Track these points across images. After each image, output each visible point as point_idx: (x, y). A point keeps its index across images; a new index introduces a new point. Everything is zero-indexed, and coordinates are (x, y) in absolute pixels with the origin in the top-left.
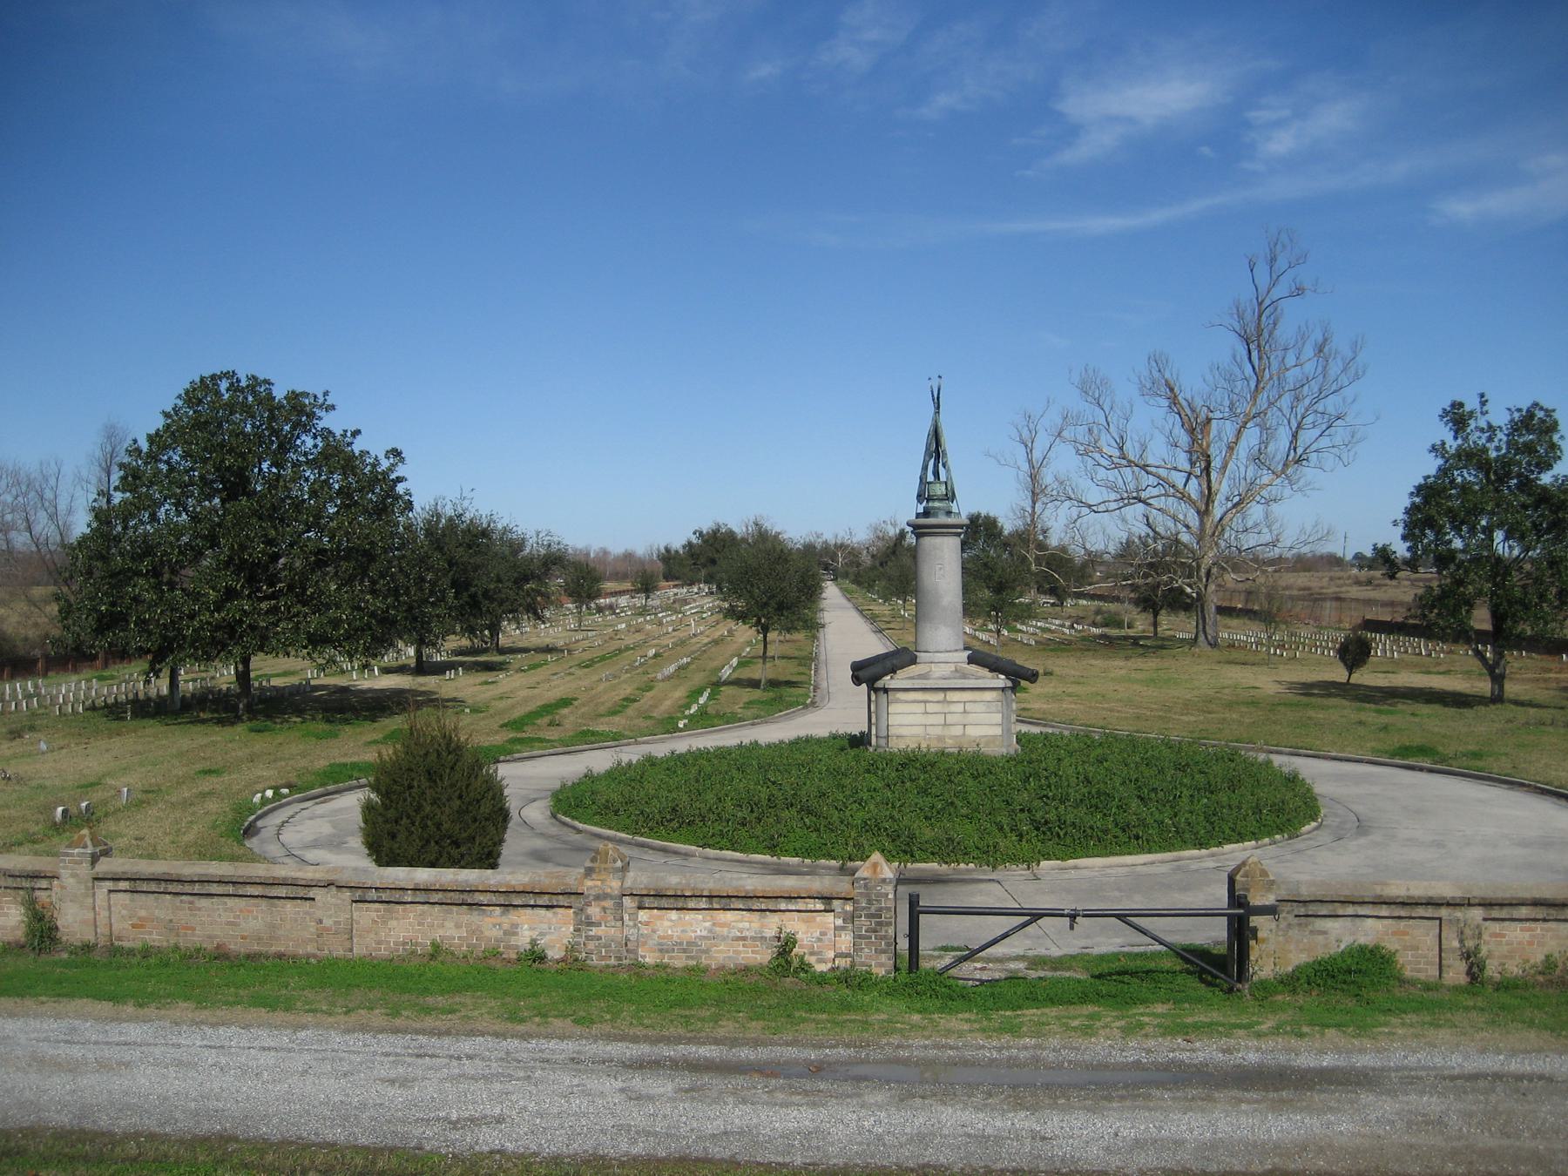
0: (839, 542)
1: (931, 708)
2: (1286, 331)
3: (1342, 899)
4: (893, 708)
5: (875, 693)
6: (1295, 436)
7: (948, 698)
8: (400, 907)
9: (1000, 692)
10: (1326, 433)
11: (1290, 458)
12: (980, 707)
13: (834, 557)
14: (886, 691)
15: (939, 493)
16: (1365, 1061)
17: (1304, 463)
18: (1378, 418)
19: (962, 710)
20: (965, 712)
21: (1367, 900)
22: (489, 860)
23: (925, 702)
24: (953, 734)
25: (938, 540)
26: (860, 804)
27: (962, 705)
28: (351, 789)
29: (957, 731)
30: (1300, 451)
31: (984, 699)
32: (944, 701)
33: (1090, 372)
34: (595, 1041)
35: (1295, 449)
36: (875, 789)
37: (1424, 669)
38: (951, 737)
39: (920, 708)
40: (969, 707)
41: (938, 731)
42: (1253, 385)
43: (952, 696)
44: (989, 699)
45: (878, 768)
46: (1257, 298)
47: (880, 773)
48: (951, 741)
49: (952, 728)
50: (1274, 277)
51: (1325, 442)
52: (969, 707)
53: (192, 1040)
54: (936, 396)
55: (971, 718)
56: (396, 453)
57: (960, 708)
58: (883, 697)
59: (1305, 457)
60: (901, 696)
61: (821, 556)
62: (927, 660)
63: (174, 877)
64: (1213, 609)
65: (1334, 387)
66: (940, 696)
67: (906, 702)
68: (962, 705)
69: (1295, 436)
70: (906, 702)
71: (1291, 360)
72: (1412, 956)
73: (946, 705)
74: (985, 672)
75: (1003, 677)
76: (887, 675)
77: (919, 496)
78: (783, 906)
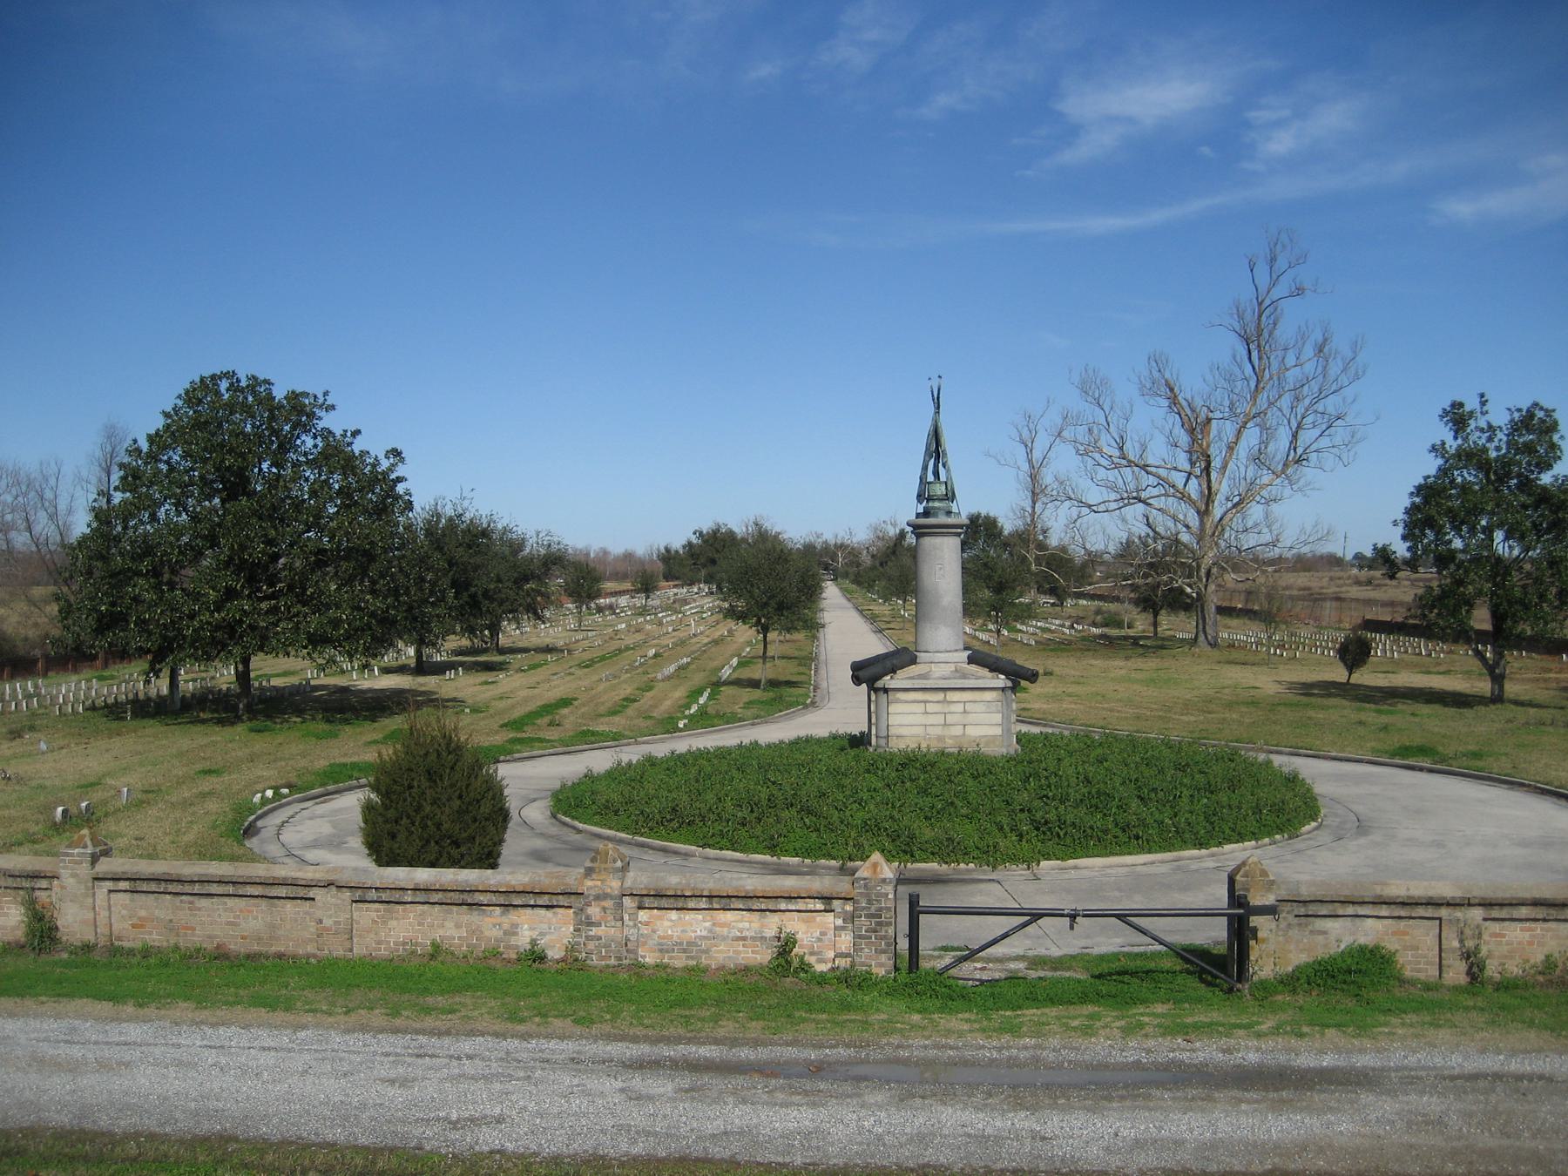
0: (839, 542)
1: (931, 708)
2: (1286, 331)
4: (893, 708)
5: (875, 693)
7: (948, 698)
9: (1000, 692)
10: (1326, 433)
11: (1290, 458)
12: (980, 707)
13: (834, 557)
14: (886, 691)
15: (939, 493)
17: (1304, 463)
18: (1378, 418)
19: (962, 710)
20: (965, 712)
23: (925, 702)
24: (953, 734)
25: (938, 540)
26: (860, 804)
27: (962, 705)
30: (1300, 451)
31: (984, 699)
32: (944, 701)
33: (1090, 372)
35: (1295, 449)
36: (875, 789)
38: (951, 737)
39: (920, 708)
40: (969, 707)
42: (1253, 385)
44: (989, 699)
45: (878, 768)
46: (1257, 298)
48: (951, 741)
49: (952, 728)
50: (1274, 277)
51: (1325, 442)
52: (969, 707)
54: (936, 396)
57: (960, 708)
58: (883, 697)
60: (901, 696)
61: (821, 556)
62: (927, 660)
64: (1213, 609)
65: (1334, 387)
66: (940, 696)
67: (906, 702)
68: (962, 705)
69: (1295, 436)
70: (906, 702)
73: (946, 705)
74: (985, 672)
75: (1003, 677)
76: (887, 675)
77: (919, 496)
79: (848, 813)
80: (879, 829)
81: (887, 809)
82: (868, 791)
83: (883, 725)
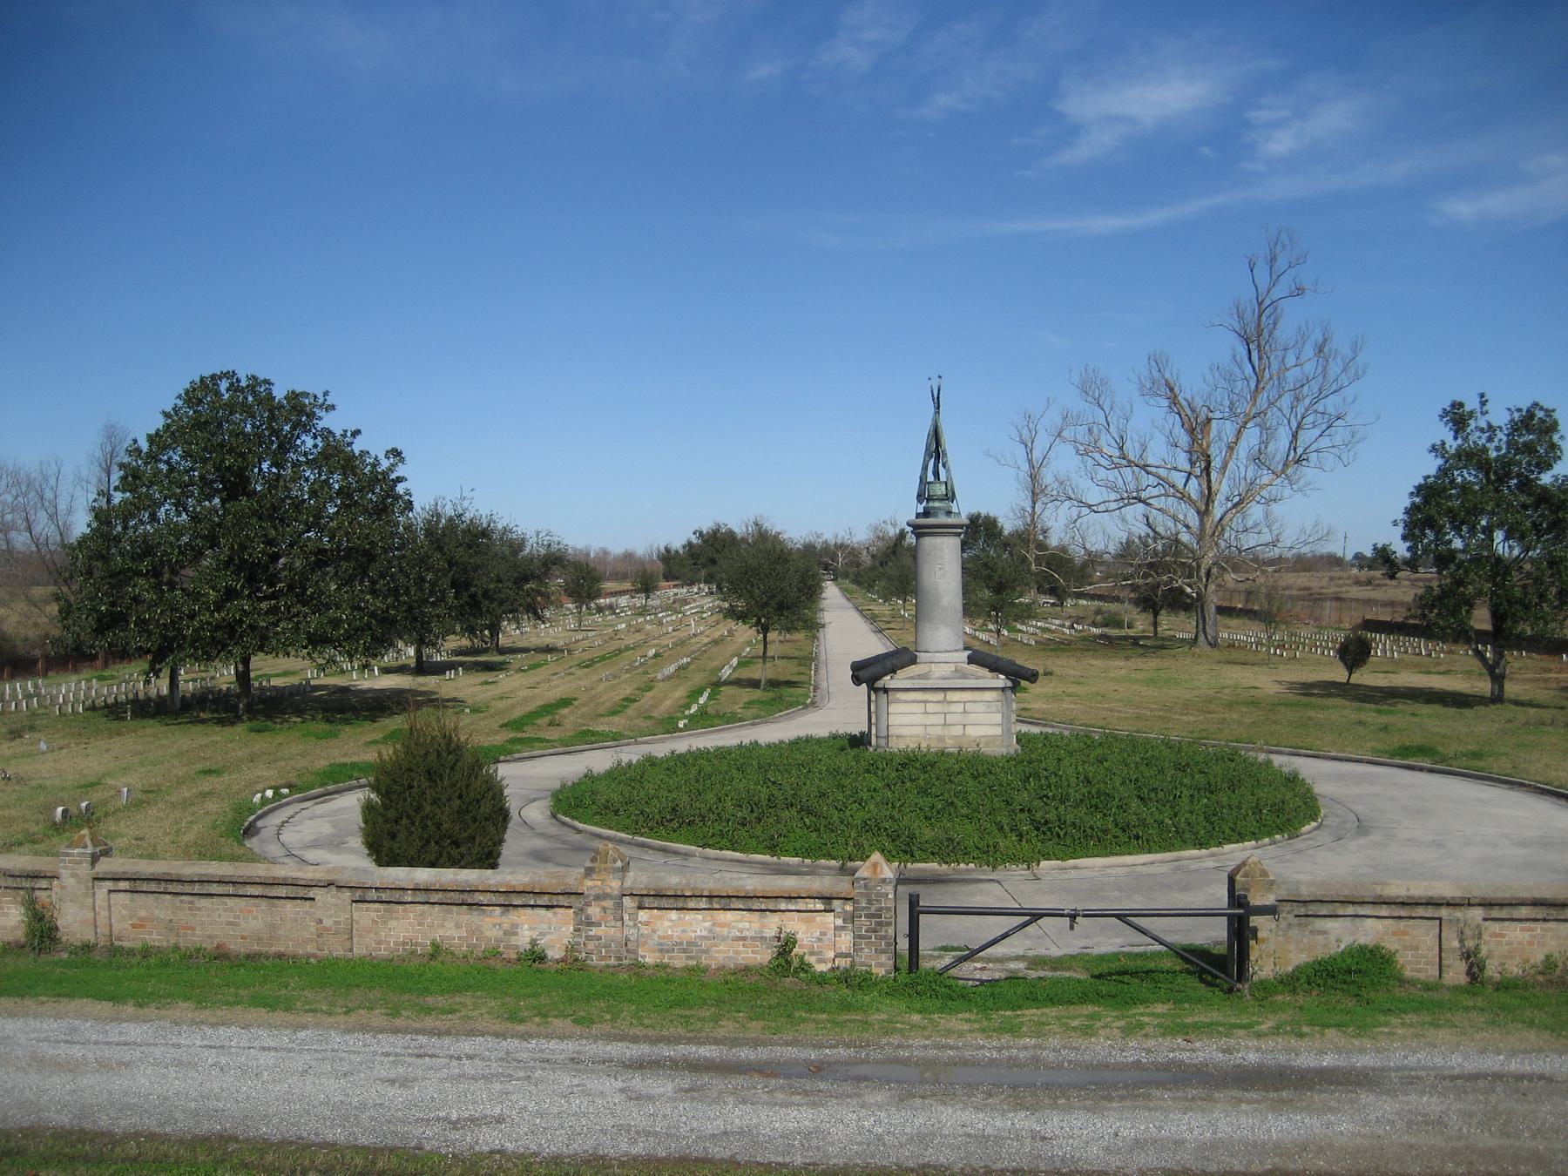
0: (839, 542)
1: (931, 708)
2: (1286, 331)
3: (1342, 899)
4: (893, 708)
5: (875, 693)
6: (1295, 436)
7: (948, 698)
8: (400, 907)
9: (1000, 692)
10: (1326, 433)
12: (980, 707)
13: (834, 557)
14: (886, 691)
15: (939, 493)
16: (1365, 1061)
17: (1304, 463)
18: (1378, 418)
19: (962, 710)
20: (965, 712)
21: (1367, 900)
22: (489, 860)
23: (925, 702)
24: (953, 734)
25: (938, 540)
26: (860, 804)
27: (962, 705)
28: (351, 789)
29: (957, 731)
30: (1300, 451)
31: (984, 699)
32: (944, 701)
33: (1090, 372)
34: (595, 1041)
35: (1295, 449)
36: (875, 789)
37: (1424, 669)
38: (951, 737)
39: (920, 708)
40: (969, 707)
41: (938, 731)
42: (1253, 385)
43: (952, 696)
44: (989, 699)
45: (878, 768)
46: (1257, 298)
47: (880, 773)
48: (951, 741)
49: (952, 728)
50: (1274, 277)
51: (1325, 442)
52: (969, 707)
53: (192, 1040)
54: (936, 396)
55: (971, 718)
56: (396, 453)
57: (960, 708)
58: (883, 697)
60: (901, 696)
61: (821, 556)
62: (927, 660)
63: (174, 877)
64: (1213, 609)
65: (1334, 387)
66: (940, 696)
67: (906, 702)
68: (962, 705)
69: (1295, 436)
70: (906, 702)
72: (1412, 956)
73: (946, 705)
74: (985, 672)
75: (1003, 677)
77: (919, 496)
78: (783, 906)
80: (879, 829)
82: (868, 791)
83: (883, 725)
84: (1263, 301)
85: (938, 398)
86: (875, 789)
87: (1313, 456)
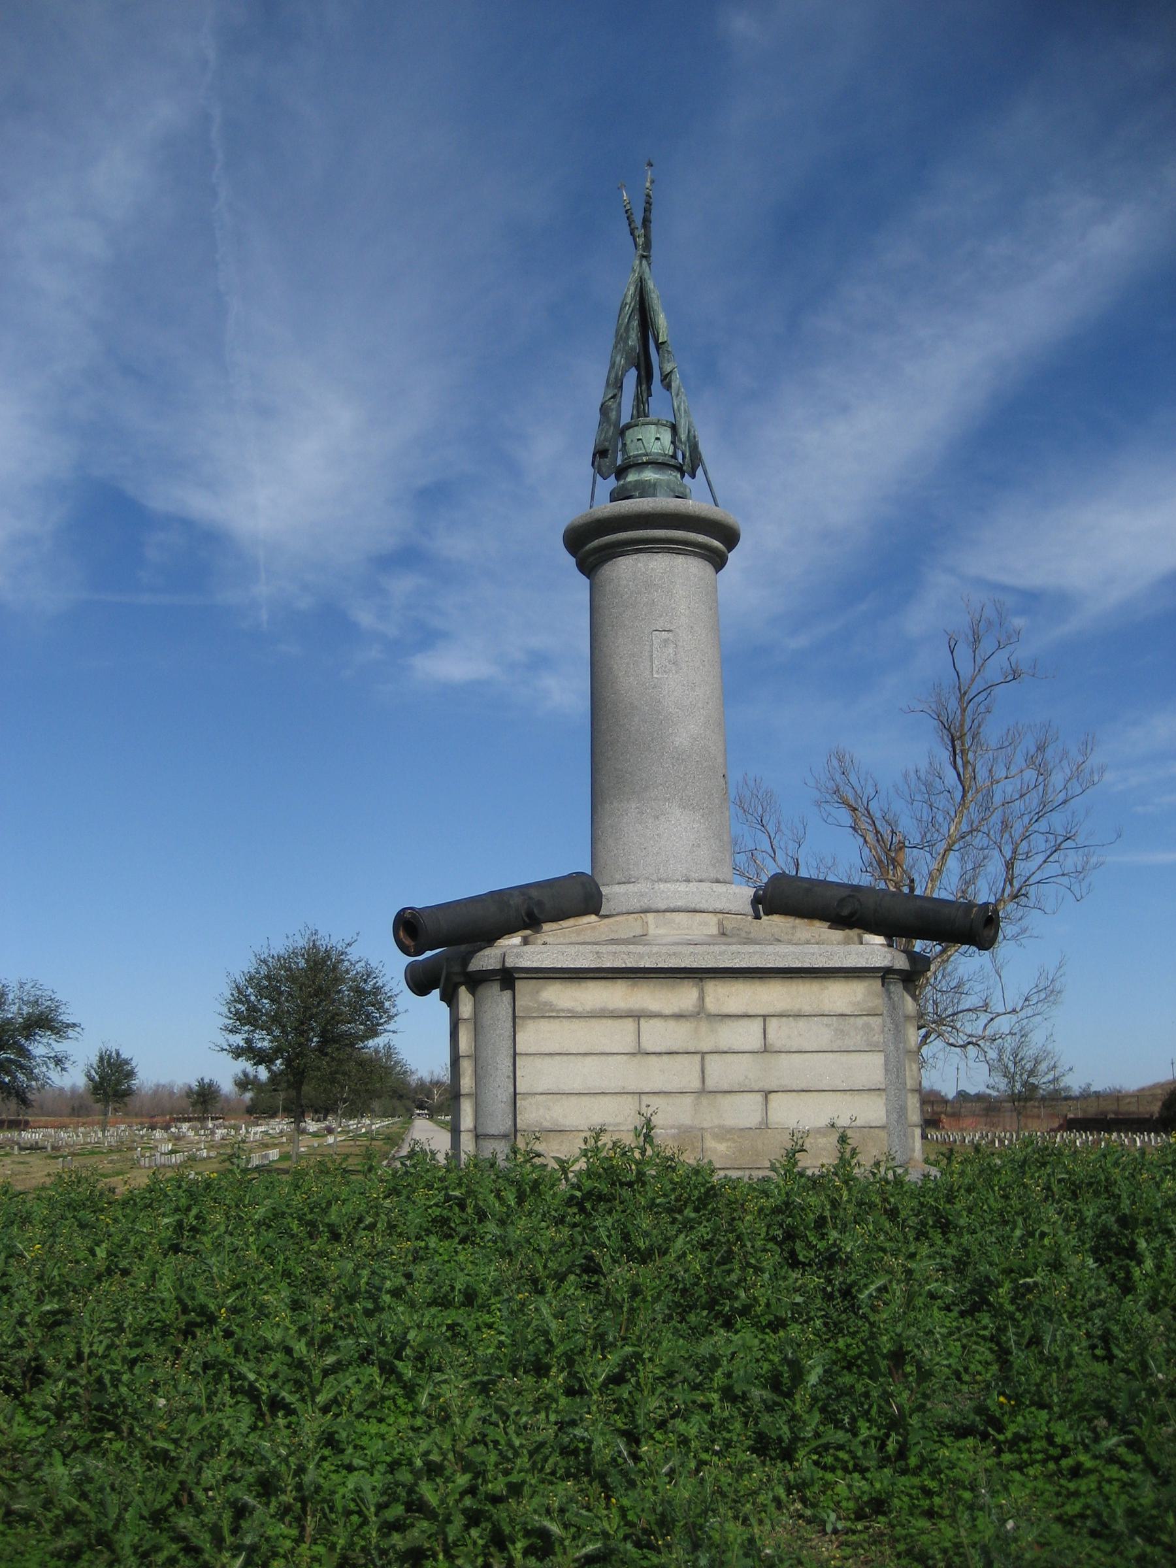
0: (435, 1078)
1: (656, 1035)
2: (992, 733)
4: (531, 1037)
5: (472, 991)
6: (1009, 865)
7: (711, 1005)
9: (877, 985)
10: (1051, 859)
11: (1006, 895)
12: (817, 1034)
13: (429, 1095)
14: (507, 978)
15: (655, 448)
17: (1023, 900)
18: (1119, 836)
19: (756, 1043)
20: (766, 1050)
23: (637, 1016)
24: (730, 1121)
25: (656, 565)
26: (388, 1370)
27: (756, 1026)
30: (1016, 885)
31: (827, 1007)
32: (700, 1014)
33: (751, 783)
35: (1011, 884)
36: (470, 1297)
38: (725, 1133)
39: (620, 1035)
40: (779, 1033)
42: (958, 795)
44: (841, 1006)
45: (482, 1216)
46: (959, 688)
47: (492, 1227)
48: (722, 1147)
49: (726, 1101)
50: (979, 661)
51: (1051, 869)
52: (779, 1033)
54: (638, 221)
55: (785, 1070)
57: (748, 1035)
58: (497, 1001)
59: (1023, 891)
60: (557, 994)
61: (416, 1093)
62: (636, 904)
64: (550, 1318)
65: (1062, 796)
66: (685, 996)
67: (574, 1016)
68: (756, 1026)
69: (1009, 865)
70: (574, 1016)
71: (1000, 773)
73: (704, 1026)
74: (820, 929)
75: (880, 940)
76: (510, 931)
77: (601, 453)
79: (312, 1424)
80: (499, 1541)
81: (542, 1403)
82: (442, 1302)
83: (498, 1093)
84: (965, 693)
85: (646, 222)
86: (470, 1297)
87: (1032, 890)
